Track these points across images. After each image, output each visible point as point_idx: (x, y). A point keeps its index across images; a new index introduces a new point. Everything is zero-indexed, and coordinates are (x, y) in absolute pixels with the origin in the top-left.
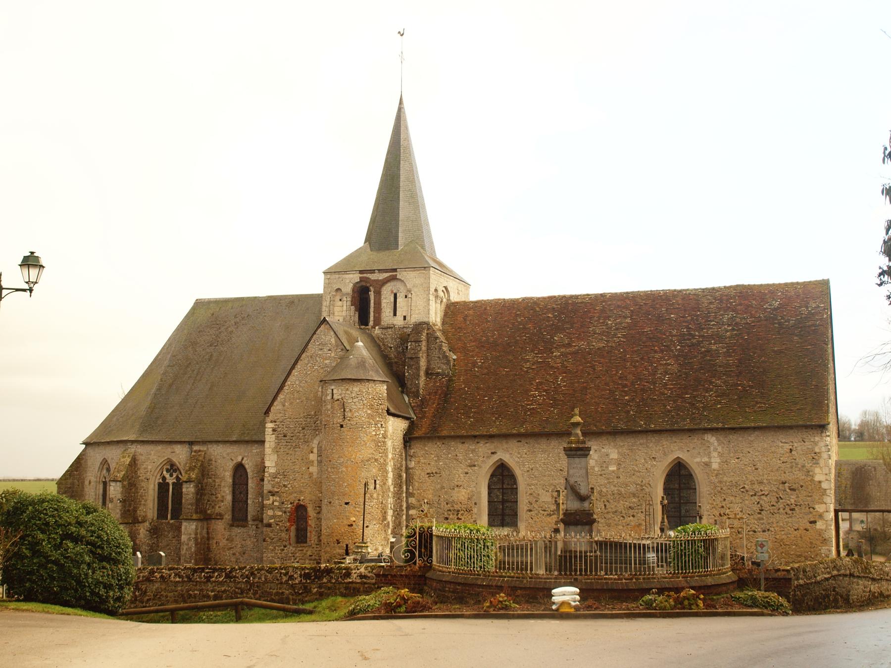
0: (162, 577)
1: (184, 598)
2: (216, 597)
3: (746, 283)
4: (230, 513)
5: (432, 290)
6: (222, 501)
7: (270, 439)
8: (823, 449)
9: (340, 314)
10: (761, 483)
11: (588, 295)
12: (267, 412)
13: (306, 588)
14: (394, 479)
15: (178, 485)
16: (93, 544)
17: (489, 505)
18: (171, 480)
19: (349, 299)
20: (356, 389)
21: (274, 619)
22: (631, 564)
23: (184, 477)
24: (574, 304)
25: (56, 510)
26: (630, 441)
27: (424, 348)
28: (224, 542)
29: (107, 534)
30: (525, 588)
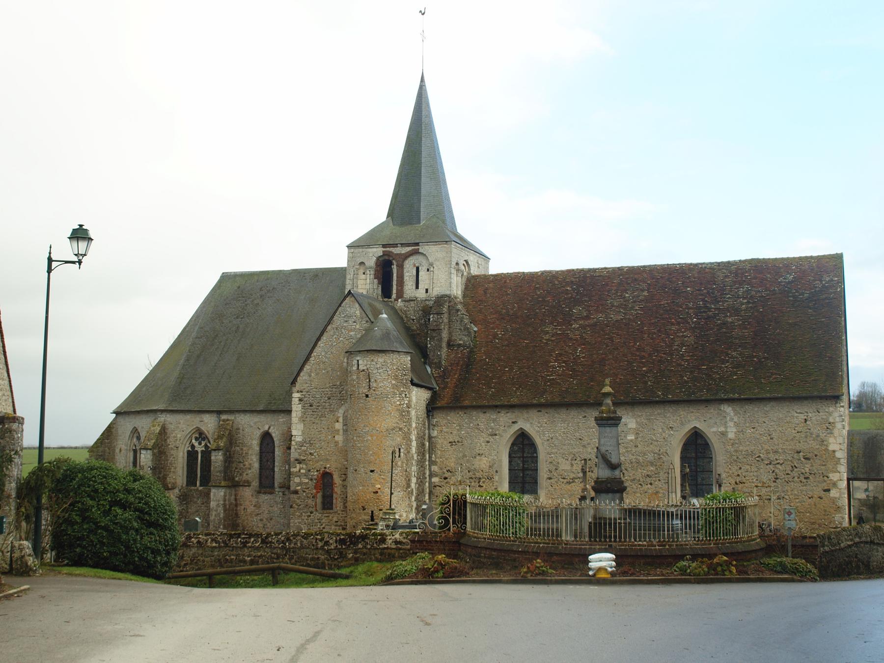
0: (199, 542)
1: (220, 562)
2: (252, 562)
3: (761, 257)
4: (257, 480)
6: (250, 469)
7: (297, 408)
8: (838, 419)
9: (363, 287)
10: (776, 452)
11: (606, 268)
12: (294, 382)
13: (341, 553)
15: (207, 453)
16: (141, 511)
17: (510, 473)
18: (199, 448)
20: (381, 360)
21: (311, 583)
22: (664, 531)
23: (212, 446)
24: (592, 277)
25: (105, 477)
26: (647, 411)
27: (446, 320)
28: (251, 509)
29: (154, 501)
30: (560, 554)
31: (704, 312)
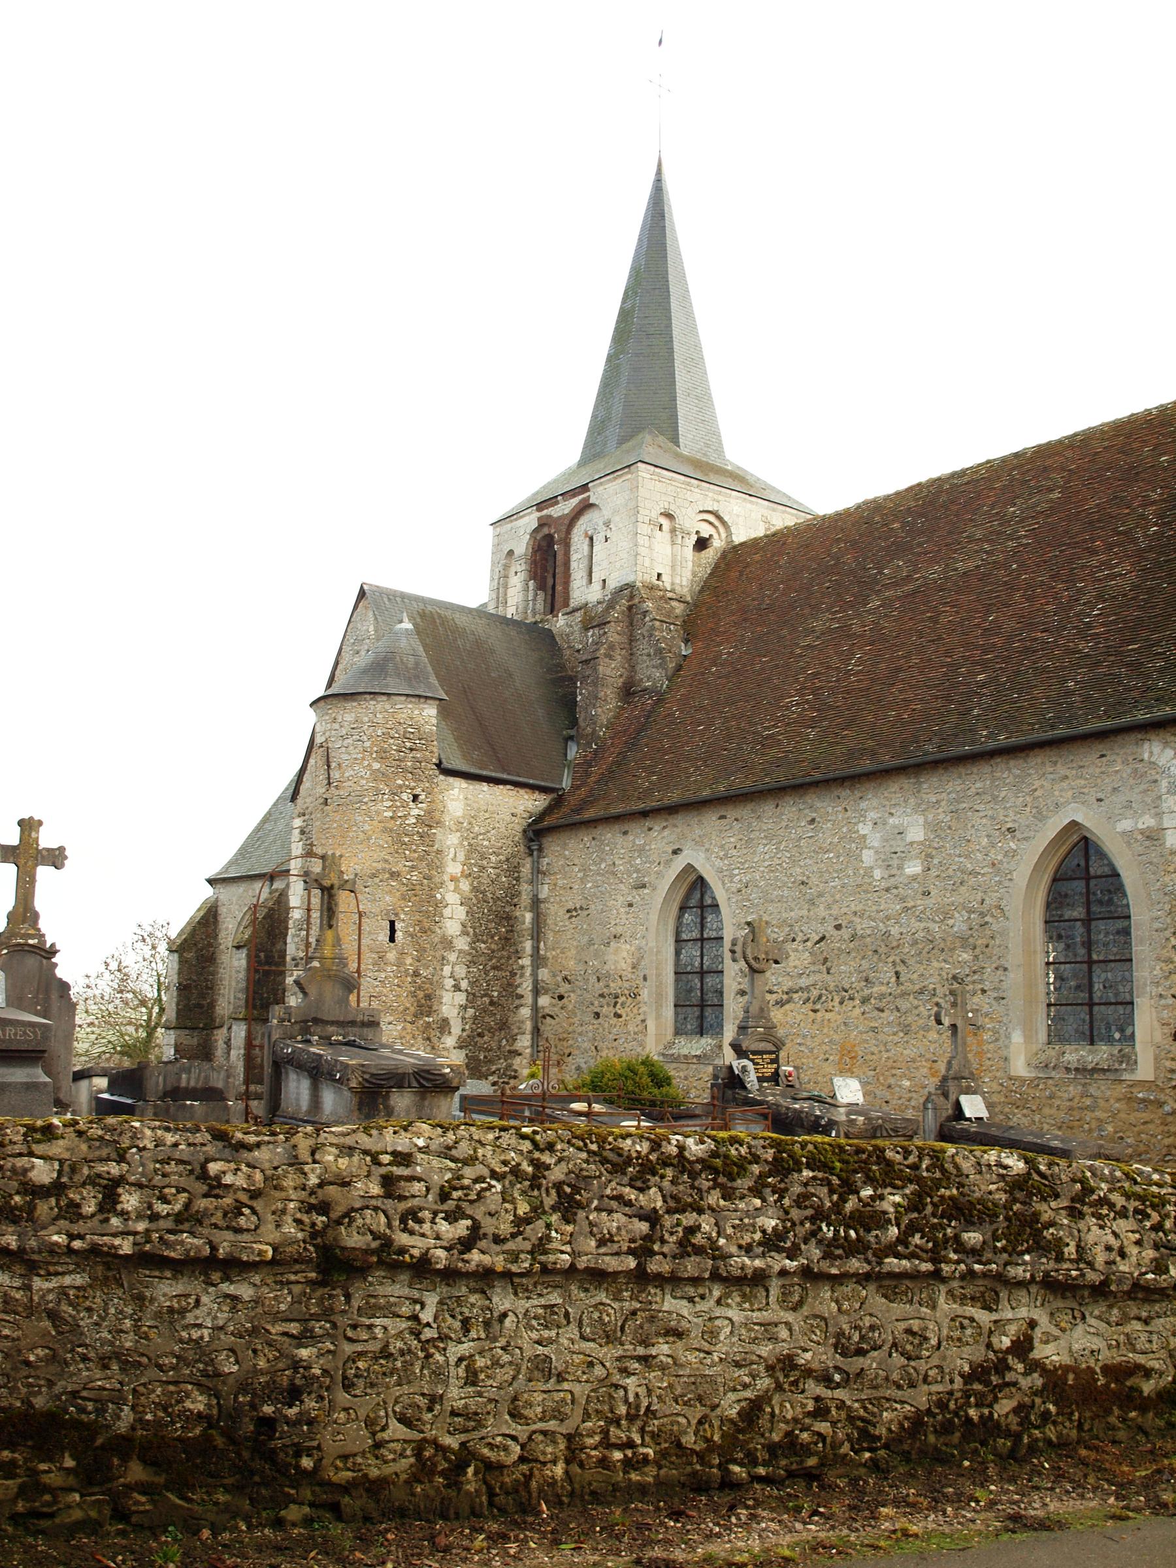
20: (349, 717)
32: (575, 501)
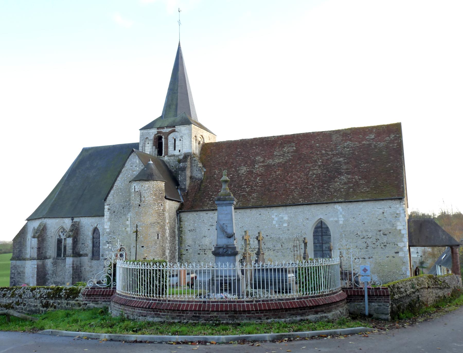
5: (193, 136)
7: (107, 213)
11: (274, 136)
12: (105, 200)
14: (170, 233)
19: (152, 142)
20: (147, 186)
31: (326, 156)
32: (170, 129)
